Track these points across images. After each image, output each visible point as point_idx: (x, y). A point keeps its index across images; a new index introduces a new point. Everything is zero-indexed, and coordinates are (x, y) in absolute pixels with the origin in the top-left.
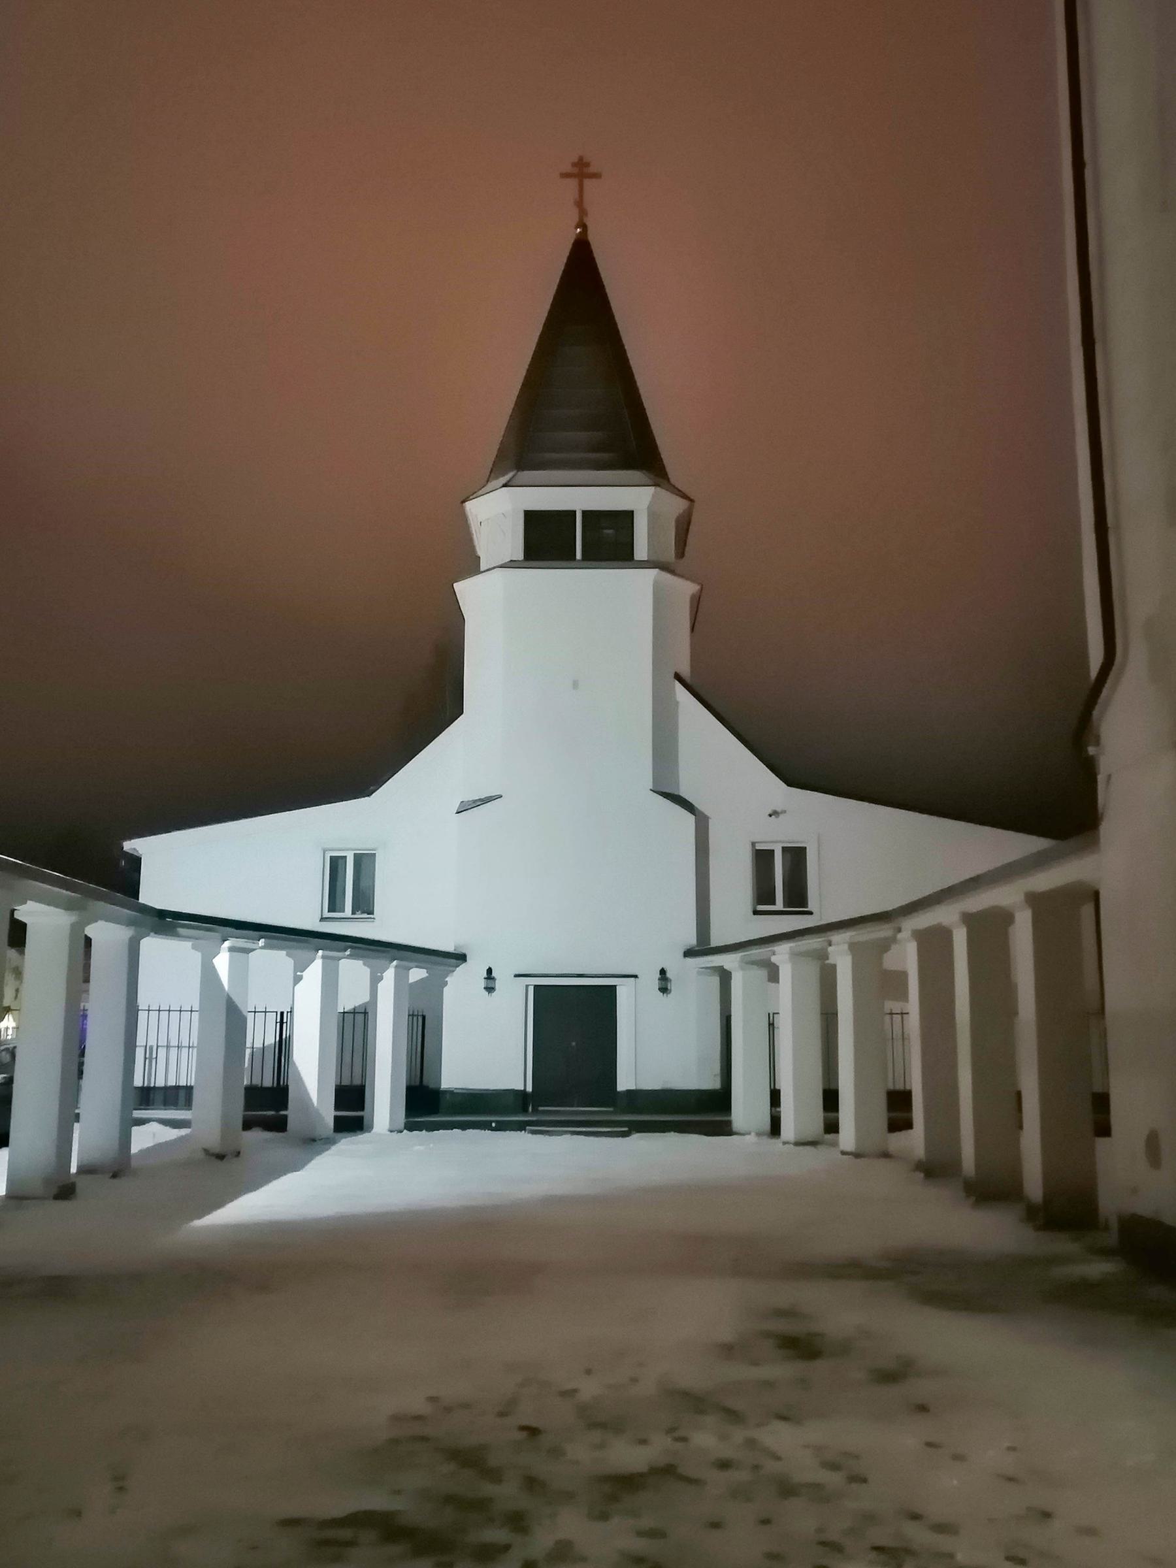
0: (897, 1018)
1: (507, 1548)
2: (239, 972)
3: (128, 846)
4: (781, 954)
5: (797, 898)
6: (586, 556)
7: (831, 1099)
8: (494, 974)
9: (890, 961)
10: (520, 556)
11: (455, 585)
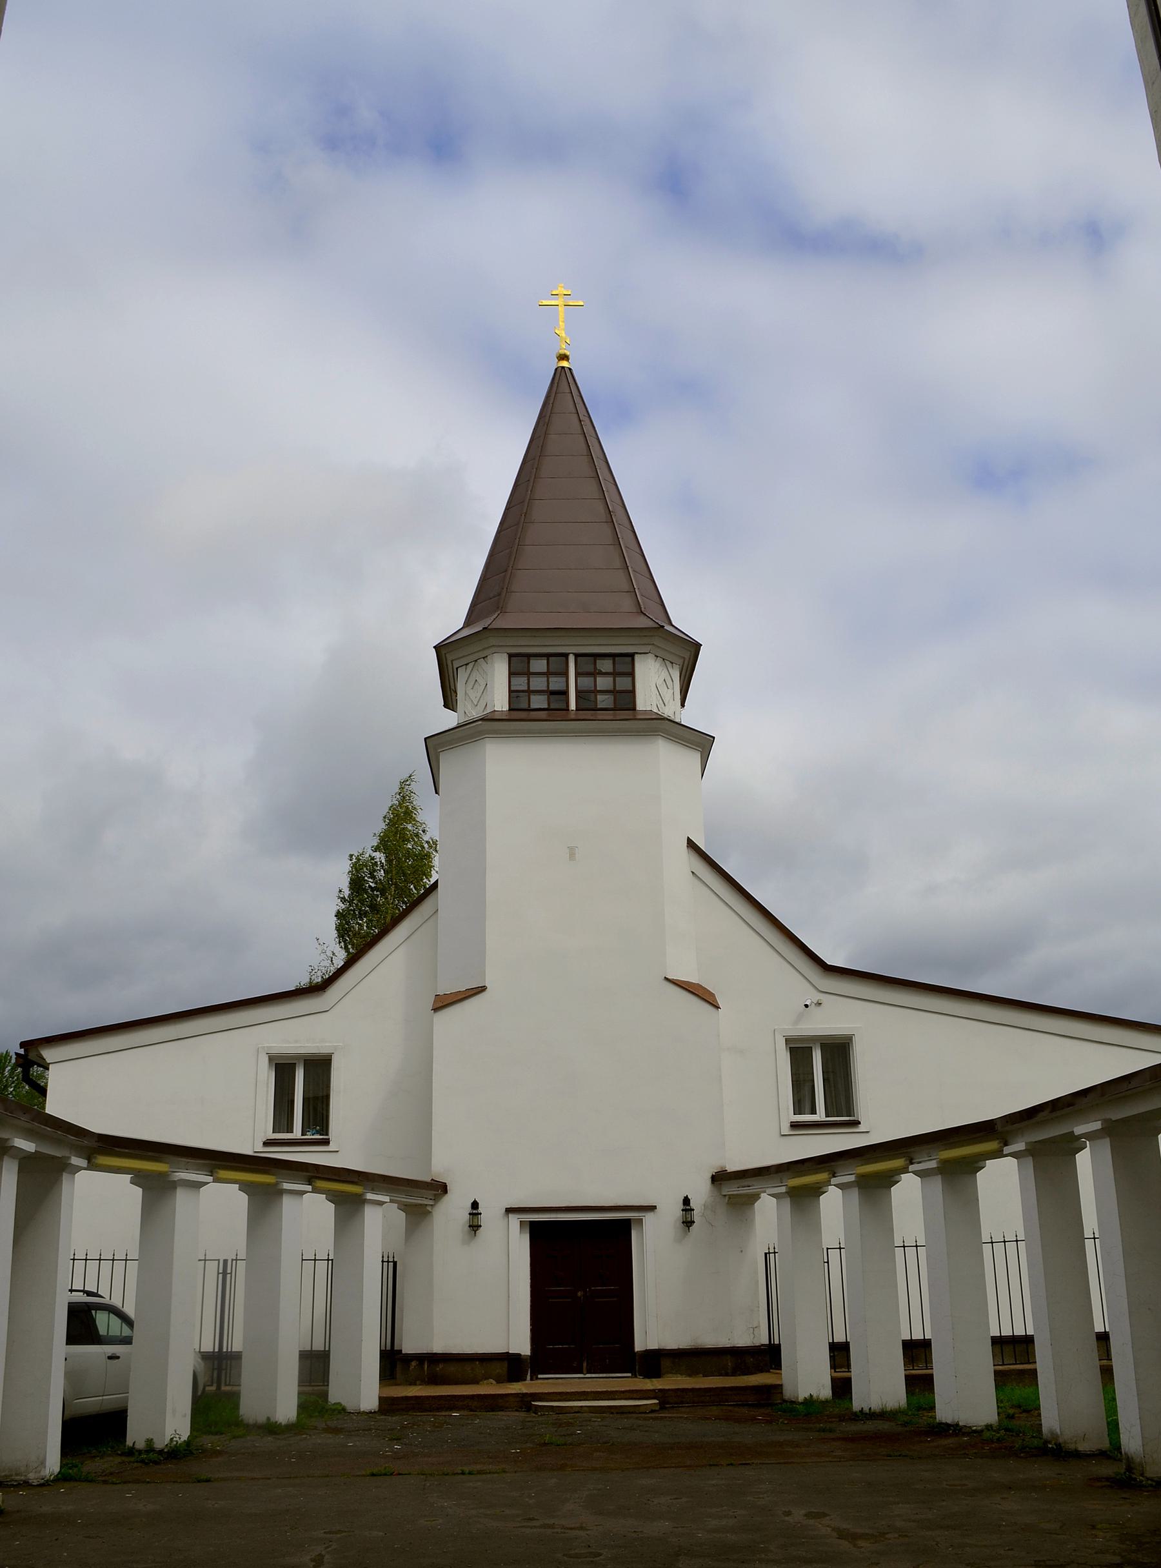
8: (480, 1210)
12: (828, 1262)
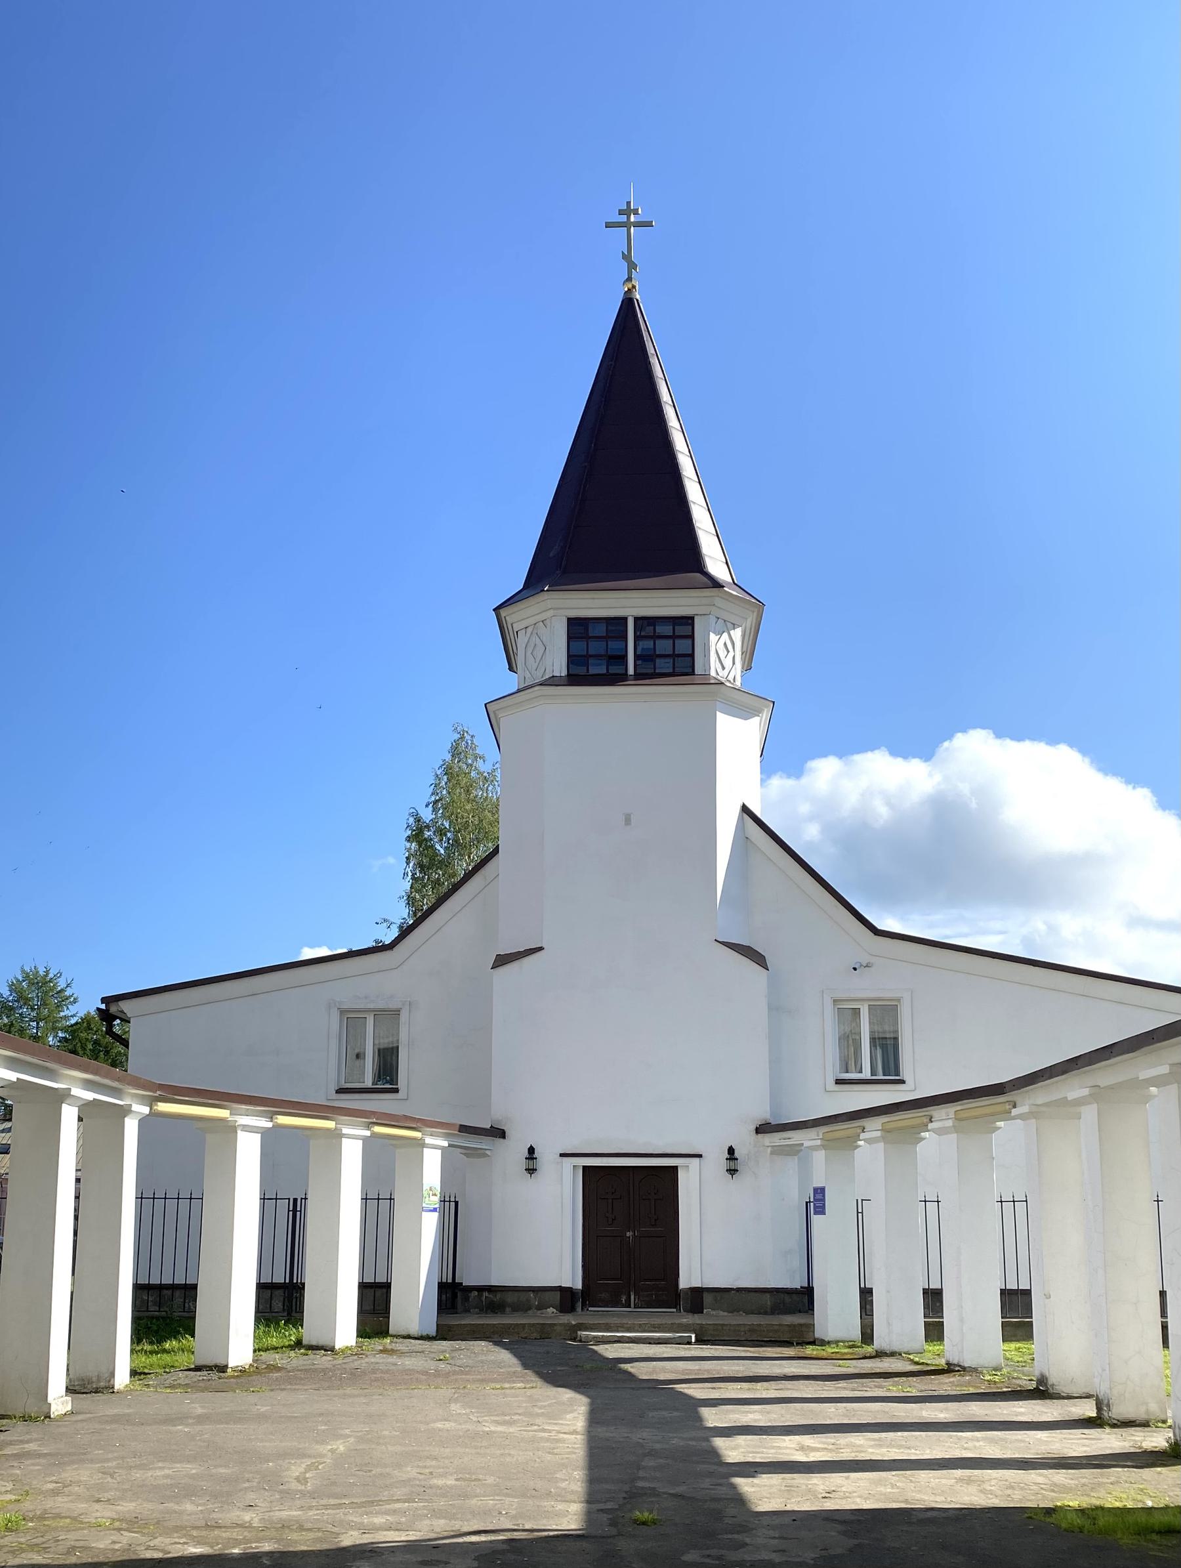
8: (736, 1155)
12: (858, 1212)
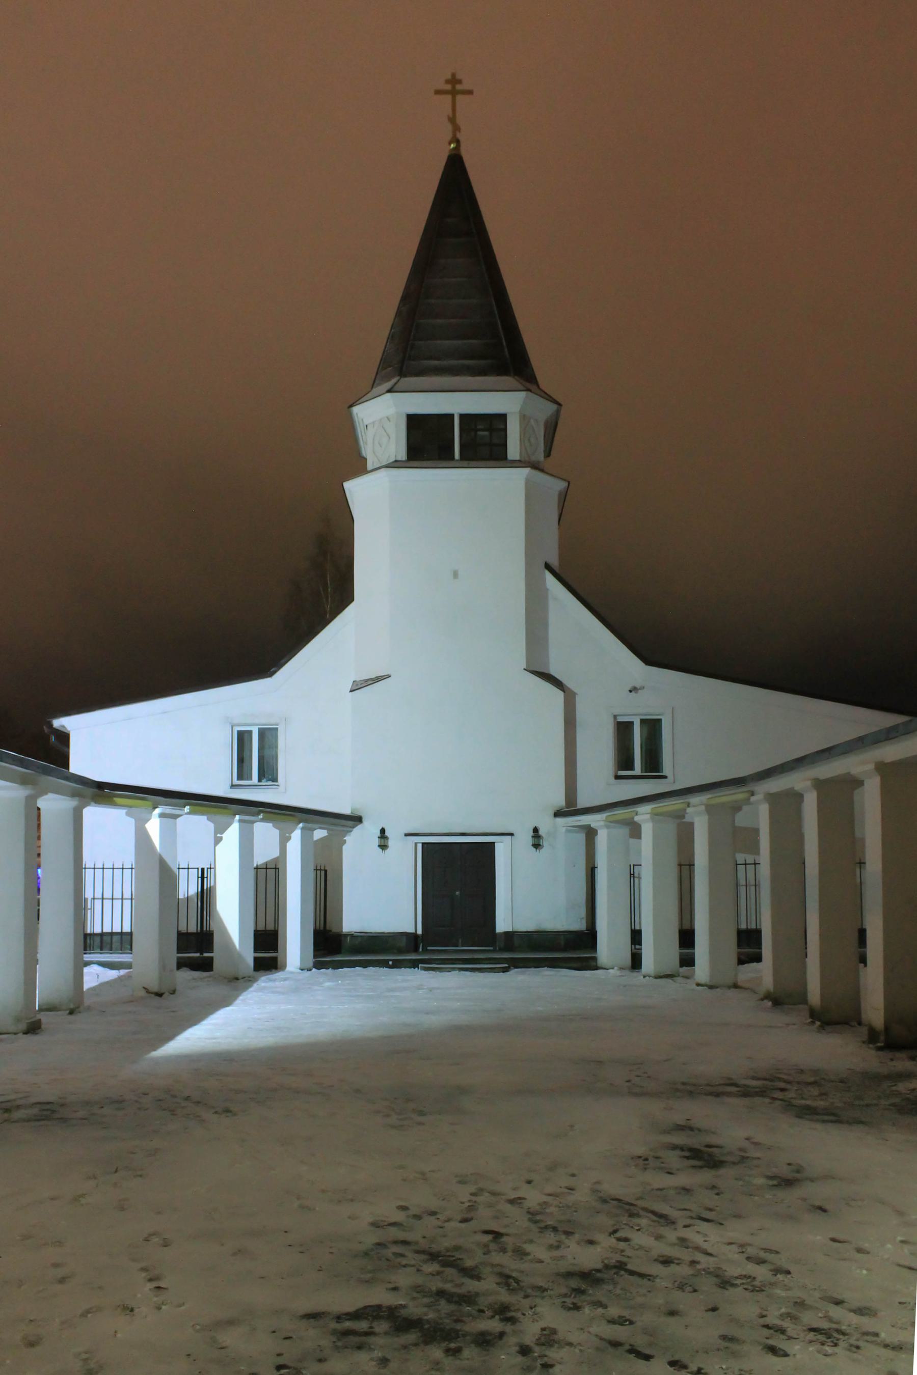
0: (751, 868)
1: (502, 1335)
2: (168, 834)
3: (58, 723)
4: (643, 814)
5: (653, 764)
6: (463, 457)
7: (687, 938)
8: (387, 834)
9: (741, 820)
10: (402, 455)
11: (347, 485)
